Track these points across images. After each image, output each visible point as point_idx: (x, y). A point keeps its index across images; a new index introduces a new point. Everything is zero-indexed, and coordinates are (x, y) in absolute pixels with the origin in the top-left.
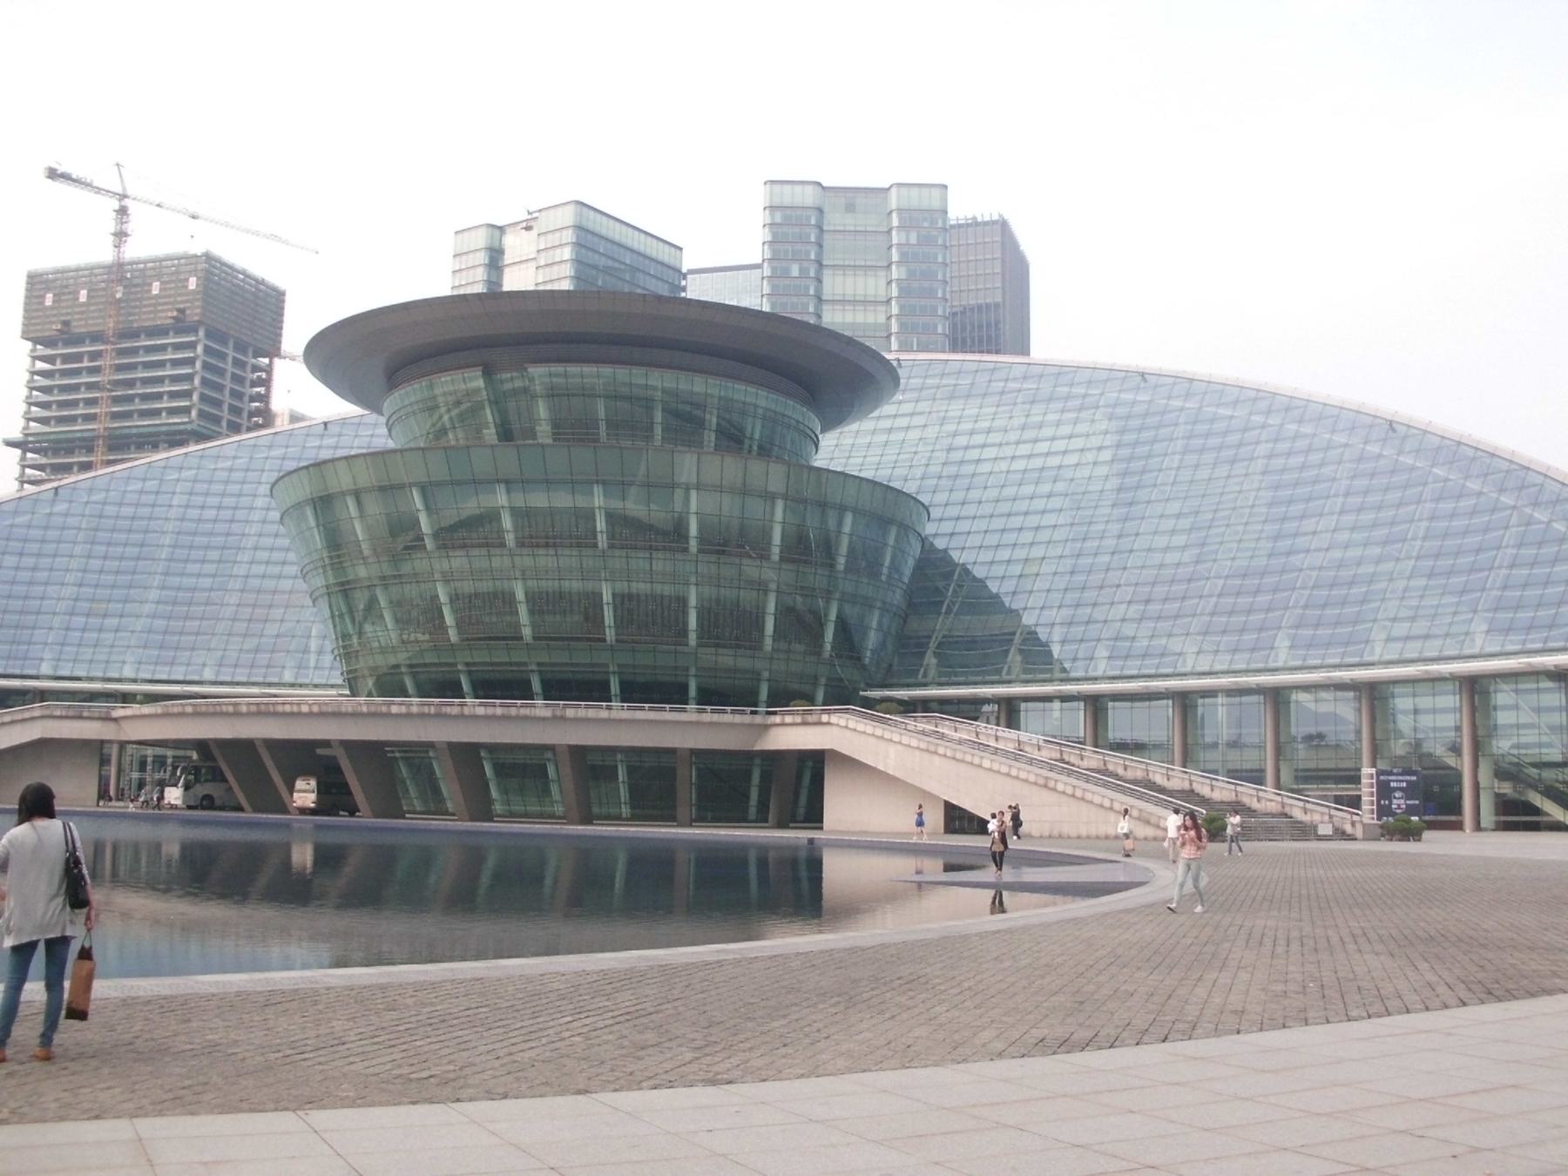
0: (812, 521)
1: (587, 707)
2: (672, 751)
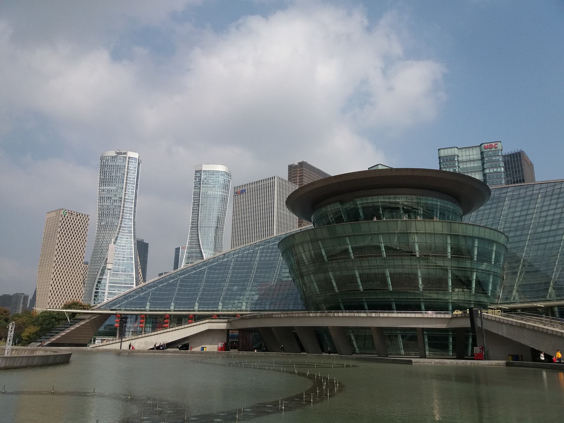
0: (462, 242)
1: (388, 313)
2: (369, 328)
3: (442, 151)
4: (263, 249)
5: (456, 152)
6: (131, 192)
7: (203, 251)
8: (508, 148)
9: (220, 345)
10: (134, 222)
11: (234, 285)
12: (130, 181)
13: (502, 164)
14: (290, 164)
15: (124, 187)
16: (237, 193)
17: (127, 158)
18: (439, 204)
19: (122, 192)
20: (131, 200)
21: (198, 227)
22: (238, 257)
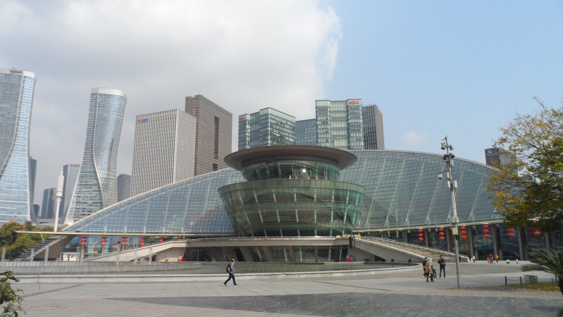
0: (341, 193)
3: (318, 102)
4: (193, 185)
5: (329, 104)
6: (26, 111)
7: (97, 170)
8: (366, 102)
9: (181, 258)
10: (29, 141)
11: (173, 214)
12: (25, 100)
13: (361, 117)
14: (188, 96)
15: (19, 105)
16: (139, 121)
17: (23, 77)
18: (327, 166)
19: (16, 110)
20: (26, 118)
21: (92, 148)
22: (173, 191)
